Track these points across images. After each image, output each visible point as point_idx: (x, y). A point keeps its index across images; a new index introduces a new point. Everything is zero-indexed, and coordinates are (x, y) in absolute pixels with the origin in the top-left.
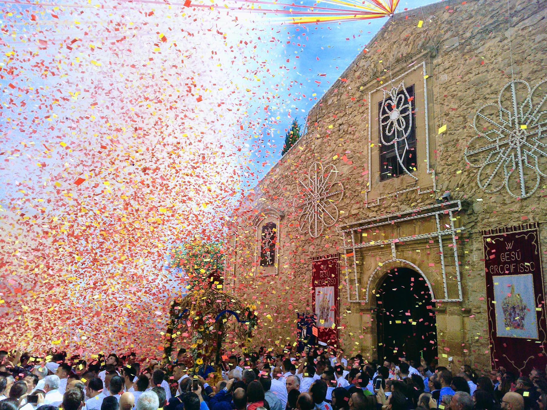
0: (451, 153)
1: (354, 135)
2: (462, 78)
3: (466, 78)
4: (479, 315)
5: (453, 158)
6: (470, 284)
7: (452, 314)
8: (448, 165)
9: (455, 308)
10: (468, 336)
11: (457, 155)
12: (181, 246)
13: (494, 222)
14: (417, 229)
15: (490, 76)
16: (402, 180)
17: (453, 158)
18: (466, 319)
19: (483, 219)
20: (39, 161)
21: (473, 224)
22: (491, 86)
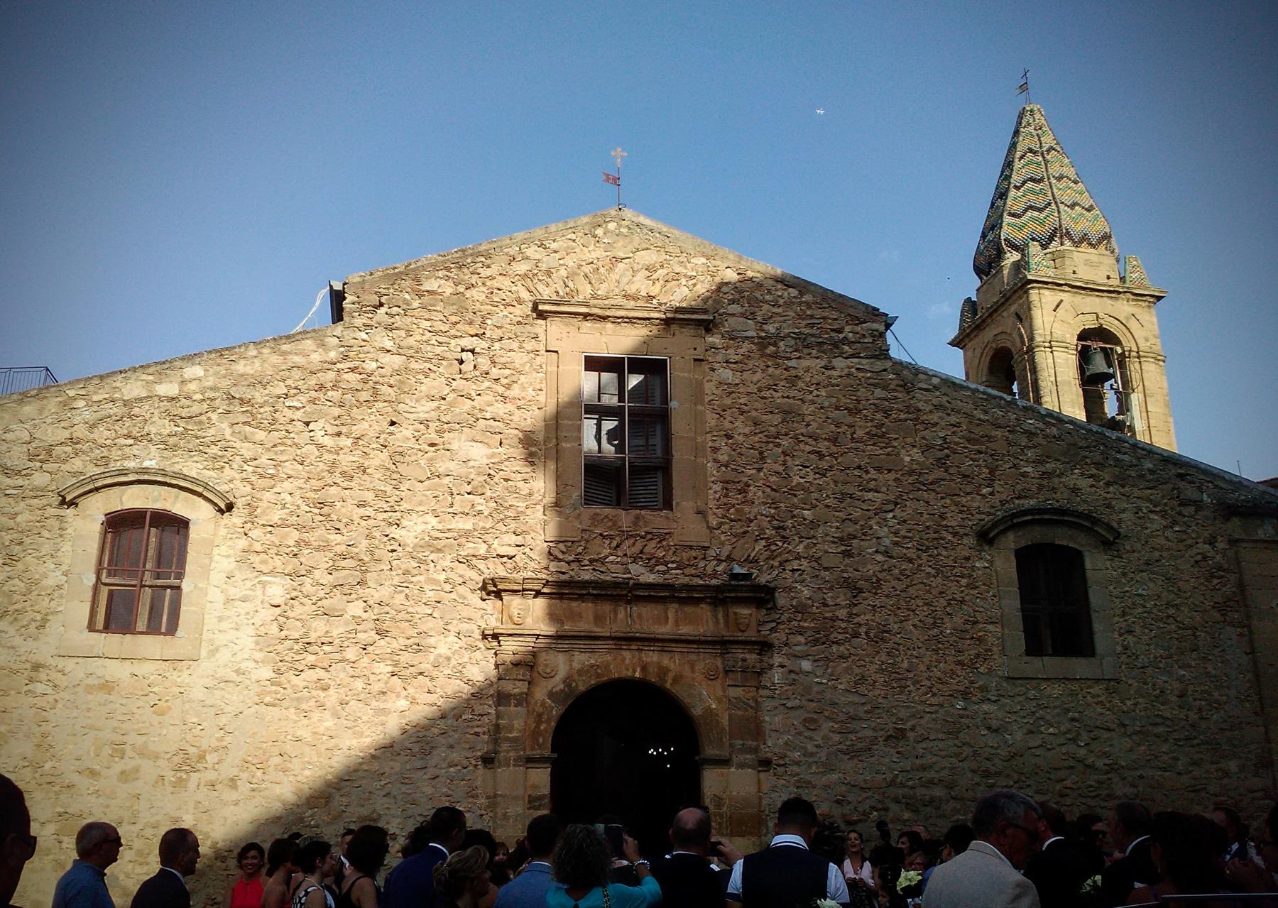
0: (734, 501)
1: (508, 387)
2: (760, 390)
3: (767, 394)
4: (782, 769)
5: (737, 510)
6: (767, 719)
7: (741, 766)
8: (732, 520)
9: (748, 756)
10: (764, 802)
11: (747, 509)
12: (741, 428)
13: (808, 628)
14: (671, 615)
15: (807, 409)
16: (637, 518)
17: (737, 510)
18: (762, 775)
19: (790, 620)
20: (228, 556)
21: (774, 625)
22: (808, 425)
